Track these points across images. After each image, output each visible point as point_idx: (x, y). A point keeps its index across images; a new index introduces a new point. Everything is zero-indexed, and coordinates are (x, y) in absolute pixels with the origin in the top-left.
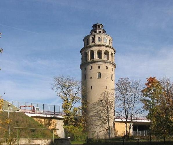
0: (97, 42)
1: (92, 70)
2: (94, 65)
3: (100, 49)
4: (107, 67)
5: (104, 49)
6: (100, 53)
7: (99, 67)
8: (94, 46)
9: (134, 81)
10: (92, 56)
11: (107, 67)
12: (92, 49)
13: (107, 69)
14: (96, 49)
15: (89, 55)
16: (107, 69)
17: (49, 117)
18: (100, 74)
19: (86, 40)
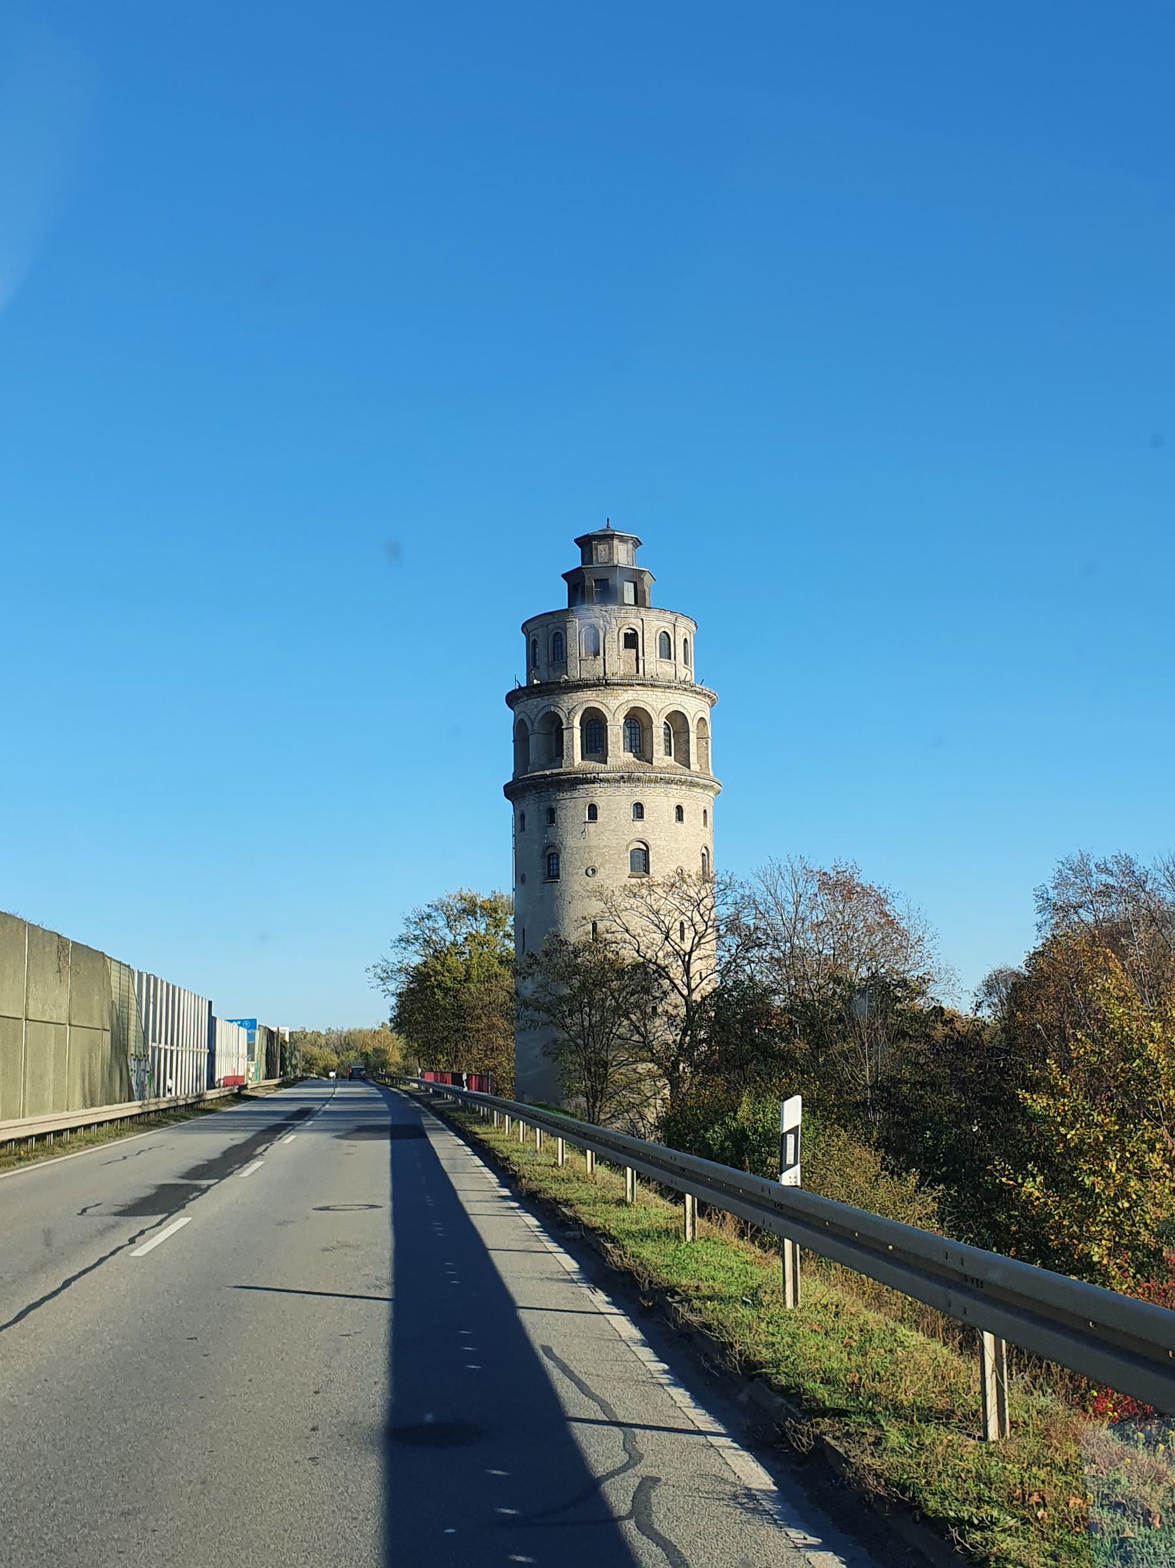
0: (618, 661)
1: (592, 827)
2: (602, 796)
3: (641, 705)
4: (679, 809)
5: (658, 704)
6: (594, 725)
7: (639, 810)
8: (603, 684)
9: (1039, 918)
10: (595, 743)
11: (679, 809)
12: (589, 699)
13: (680, 818)
14: (615, 707)
15: (577, 733)
16: (680, 818)
17: (113, 984)
18: (646, 853)
19: (546, 640)
